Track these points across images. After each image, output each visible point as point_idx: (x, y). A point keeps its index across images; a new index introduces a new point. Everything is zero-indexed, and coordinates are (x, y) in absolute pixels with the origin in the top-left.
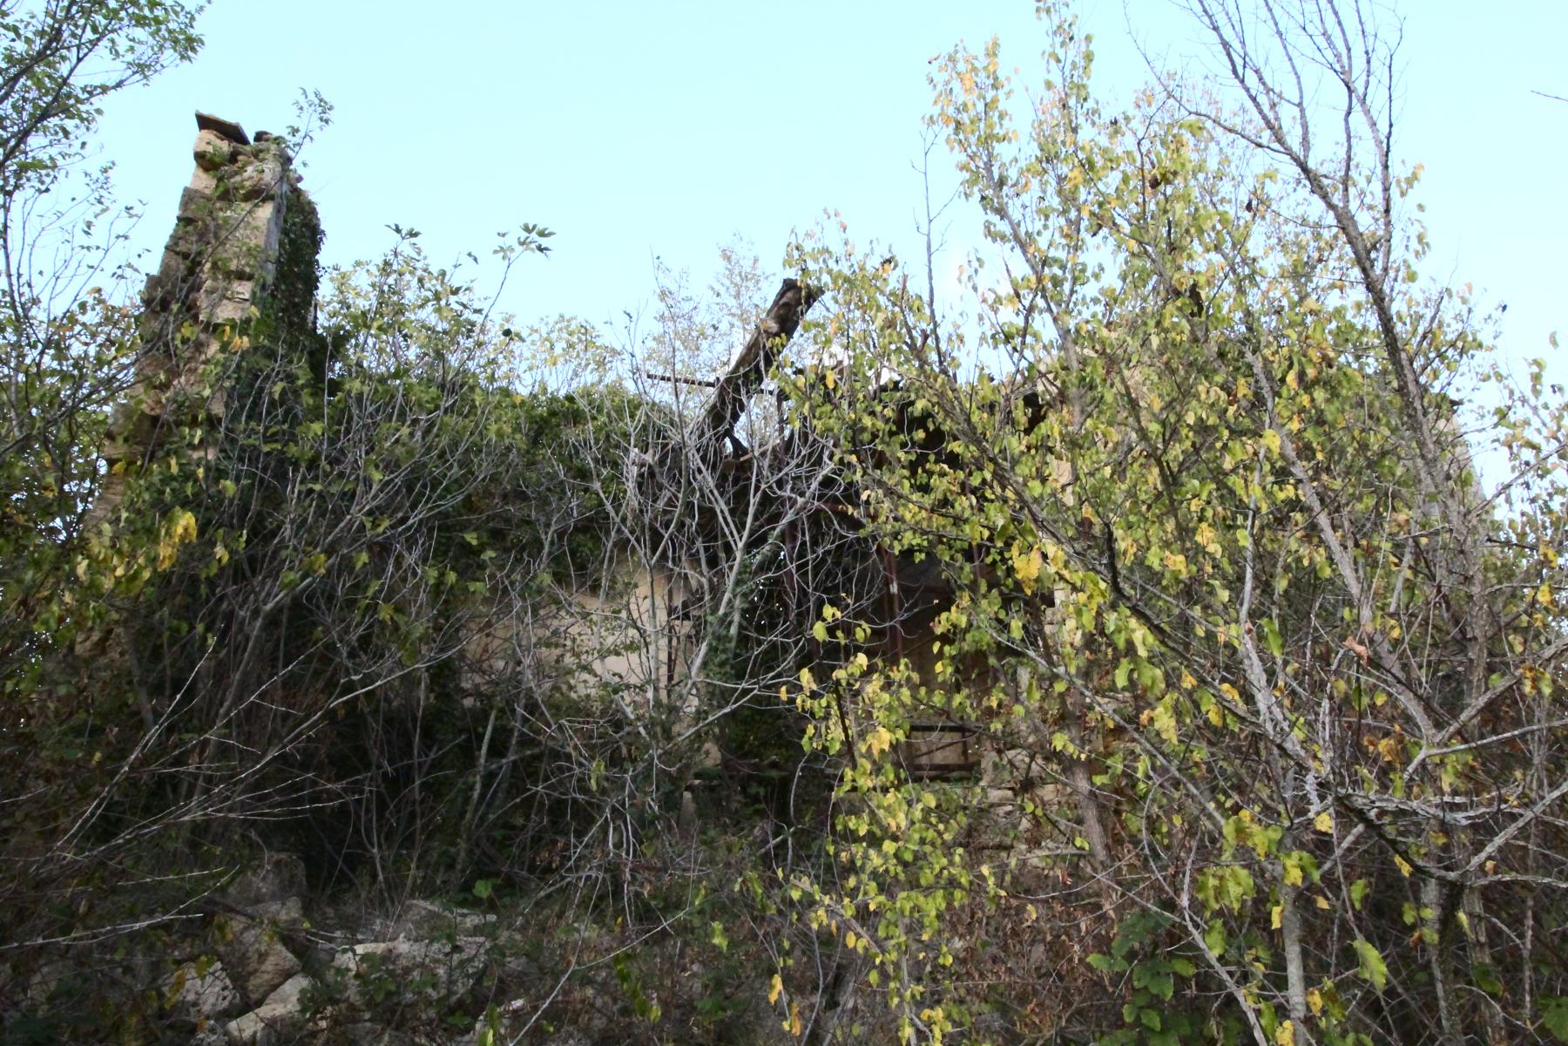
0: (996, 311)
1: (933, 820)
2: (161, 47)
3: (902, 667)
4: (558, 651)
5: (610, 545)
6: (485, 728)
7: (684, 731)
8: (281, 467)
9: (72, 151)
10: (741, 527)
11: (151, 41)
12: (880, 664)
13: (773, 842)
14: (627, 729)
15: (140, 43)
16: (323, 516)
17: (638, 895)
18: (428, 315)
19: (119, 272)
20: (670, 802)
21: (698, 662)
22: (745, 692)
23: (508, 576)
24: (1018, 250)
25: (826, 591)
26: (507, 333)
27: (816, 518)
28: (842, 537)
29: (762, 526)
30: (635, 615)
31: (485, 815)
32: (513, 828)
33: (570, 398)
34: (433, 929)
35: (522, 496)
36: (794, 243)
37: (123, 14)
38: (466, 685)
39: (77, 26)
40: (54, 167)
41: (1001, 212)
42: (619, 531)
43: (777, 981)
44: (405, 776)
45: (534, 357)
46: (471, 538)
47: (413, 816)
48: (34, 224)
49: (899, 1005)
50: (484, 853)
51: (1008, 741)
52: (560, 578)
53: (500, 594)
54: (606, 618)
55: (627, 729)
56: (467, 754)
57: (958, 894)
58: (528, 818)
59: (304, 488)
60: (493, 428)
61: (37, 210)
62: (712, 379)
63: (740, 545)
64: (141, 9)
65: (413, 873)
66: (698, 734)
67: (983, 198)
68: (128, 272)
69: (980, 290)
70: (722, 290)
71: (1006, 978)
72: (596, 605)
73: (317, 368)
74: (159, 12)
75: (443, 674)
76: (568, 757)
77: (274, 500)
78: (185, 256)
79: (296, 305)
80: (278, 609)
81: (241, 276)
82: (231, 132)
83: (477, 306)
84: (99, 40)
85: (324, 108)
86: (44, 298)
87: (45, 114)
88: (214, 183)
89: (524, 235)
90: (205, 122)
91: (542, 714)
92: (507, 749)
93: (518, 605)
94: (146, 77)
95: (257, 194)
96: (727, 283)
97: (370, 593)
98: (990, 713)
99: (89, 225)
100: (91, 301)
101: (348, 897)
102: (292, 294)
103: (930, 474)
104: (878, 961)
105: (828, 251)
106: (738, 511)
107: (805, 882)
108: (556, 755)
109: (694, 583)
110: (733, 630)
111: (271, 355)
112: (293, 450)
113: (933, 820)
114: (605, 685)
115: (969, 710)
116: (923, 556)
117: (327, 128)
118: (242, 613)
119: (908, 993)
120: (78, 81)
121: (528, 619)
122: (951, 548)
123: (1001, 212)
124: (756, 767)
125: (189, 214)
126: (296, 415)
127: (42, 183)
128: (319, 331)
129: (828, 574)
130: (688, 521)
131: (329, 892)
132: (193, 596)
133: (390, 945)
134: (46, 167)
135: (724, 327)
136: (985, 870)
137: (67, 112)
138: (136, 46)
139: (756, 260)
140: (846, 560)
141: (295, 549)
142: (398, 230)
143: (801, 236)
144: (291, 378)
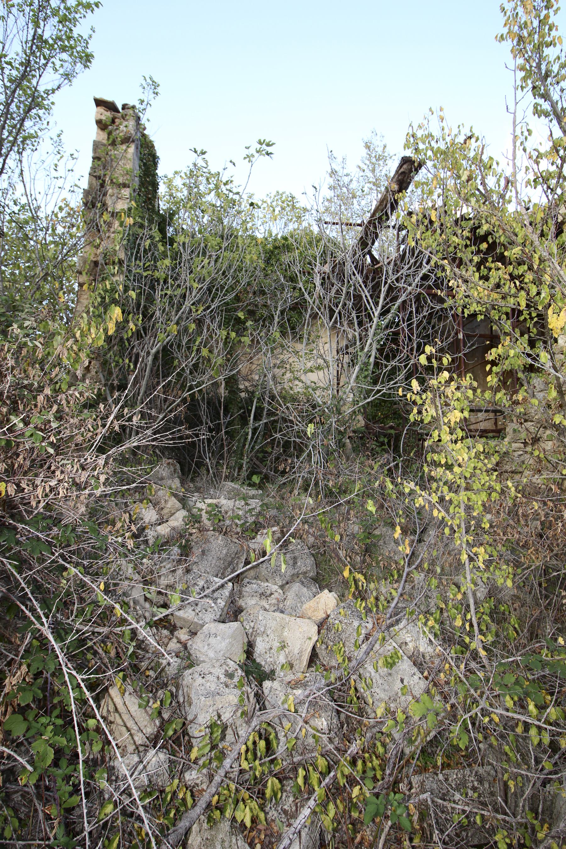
0: (537, 163)
1: (482, 458)
2: (75, 63)
3: (468, 378)
4: (284, 370)
5: (308, 316)
6: (252, 407)
7: (347, 410)
8: (153, 283)
9: (43, 127)
10: (377, 304)
11: (70, 60)
12: (455, 376)
13: (392, 465)
14: (318, 408)
15: (66, 61)
16: (173, 306)
17: (326, 486)
18: (211, 198)
19: (72, 189)
20: (341, 445)
21: (354, 376)
22: (379, 391)
23: (259, 334)
24: (555, 122)
25: (423, 338)
26: (252, 204)
27: (418, 298)
28: (432, 308)
29: (387, 303)
30: (322, 352)
31: (254, 446)
32: (266, 452)
33: (285, 239)
34: (234, 495)
35: (263, 293)
36: (411, 133)
37: (56, 46)
38: (242, 387)
39: (36, 57)
40: (37, 137)
41: (546, 96)
42: (312, 308)
43: (398, 529)
44: (218, 429)
45: (265, 217)
46: (241, 315)
47: (222, 446)
48: (34, 167)
49: (461, 545)
50: (254, 463)
51: (525, 418)
52: (283, 334)
53: (254, 342)
54: (306, 353)
55: (318, 408)
56: (244, 420)
57: (494, 495)
58: (273, 448)
59: (163, 293)
60: (248, 257)
61: (34, 160)
62: (359, 222)
63: (376, 314)
64: (63, 42)
65: (225, 471)
66: (354, 412)
67: (534, 88)
68: (76, 189)
69: (528, 152)
70: (365, 167)
71: (517, 536)
72: (300, 347)
73: (162, 231)
74: (72, 42)
75: (231, 382)
76: (291, 422)
77: (150, 299)
78: (99, 178)
79: (149, 199)
80: (157, 352)
81: (125, 186)
82: (109, 106)
83: (235, 190)
84: (47, 63)
85: (155, 85)
86: (43, 205)
87: (30, 110)
88: (106, 136)
89: (259, 146)
90: (99, 103)
91: (278, 400)
92: (262, 417)
93: (264, 349)
94: (70, 81)
95: (127, 140)
96: (368, 162)
97: (197, 343)
98: (516, 403)
99: (56, 166)
100: (63, 206)
101: (198, 479)
102: (147, 193)
103: (490, 269)
104: (449, 524)
105: (431, 136)
106: (375, 295)
107: (412, 485)
108: (285, 420)
109: (350, 336)
110: (372, 360)
111: (142, 226)
112: (157, 274)
113: (482, 458)
114: (307, 388)
115: (505, 401)
116: (483, 317)
117: (157, 98)
118: (142, 354)
119: (465, 539)
120: (41, 89)
121: (269, 355)
122: (499, 311)
123: (546, 96)
124: (382, 428)
125: (97, 155)
126: (155, 257)
127: (33, 146)
128: (161, 212)
129: (424, 328)
130: (348, 302)
131: (190, 477)
132: (121, 346)
133: (218, 500)
134: (34, 137)
135: (366, 189)
136: (510, 484)
137: (40, 106)
138: (63, 63)
139: (385, 147)
140: (433, 321)
141: (162, 323)
142: (196, 152)
143: (415, 128)
144: (151, 237)
